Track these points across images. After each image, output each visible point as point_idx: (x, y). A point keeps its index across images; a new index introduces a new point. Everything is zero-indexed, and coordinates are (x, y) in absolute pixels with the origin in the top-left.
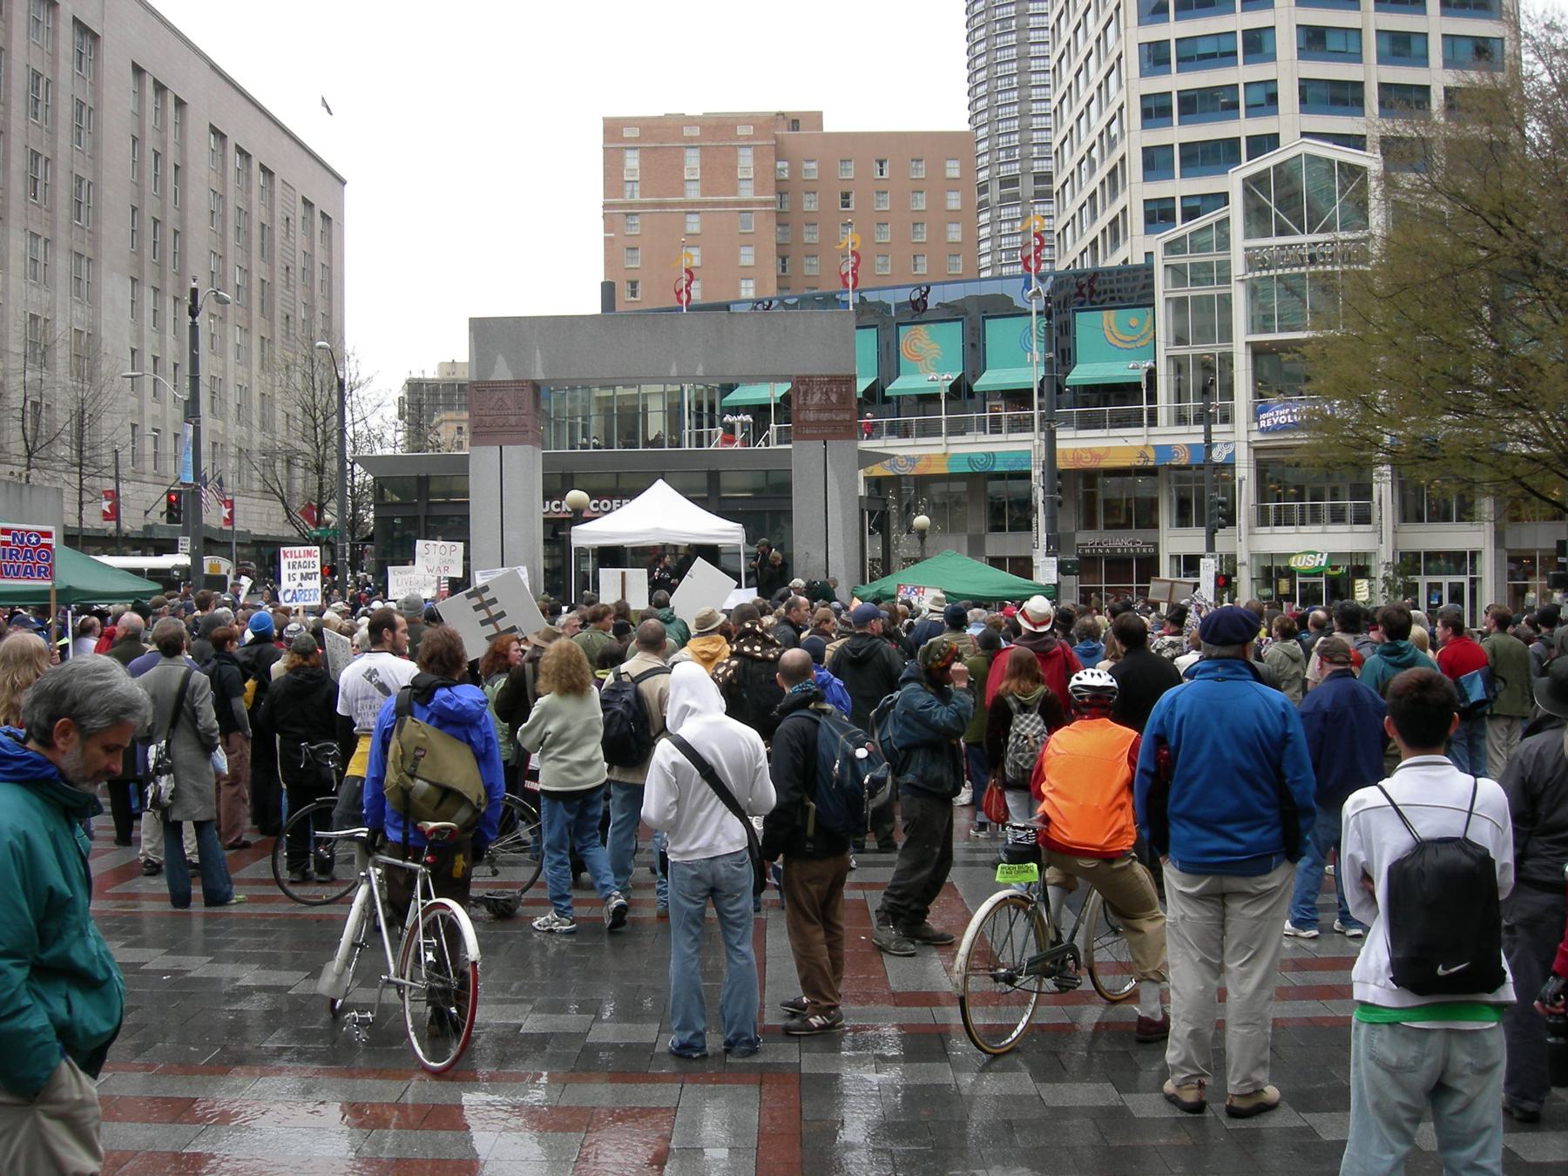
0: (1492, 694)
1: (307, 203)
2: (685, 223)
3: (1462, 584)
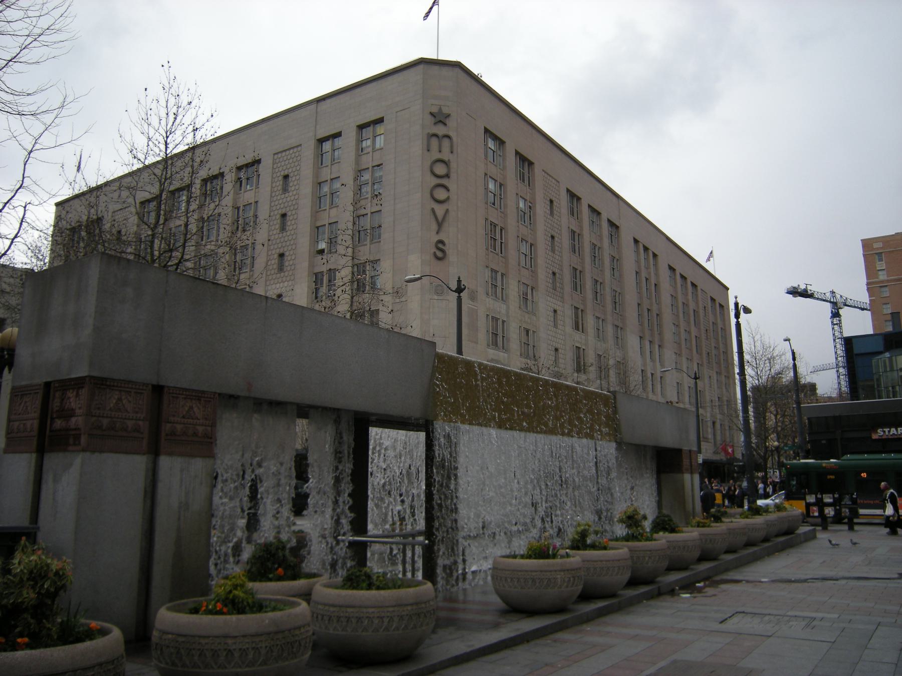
1: (713, 300)
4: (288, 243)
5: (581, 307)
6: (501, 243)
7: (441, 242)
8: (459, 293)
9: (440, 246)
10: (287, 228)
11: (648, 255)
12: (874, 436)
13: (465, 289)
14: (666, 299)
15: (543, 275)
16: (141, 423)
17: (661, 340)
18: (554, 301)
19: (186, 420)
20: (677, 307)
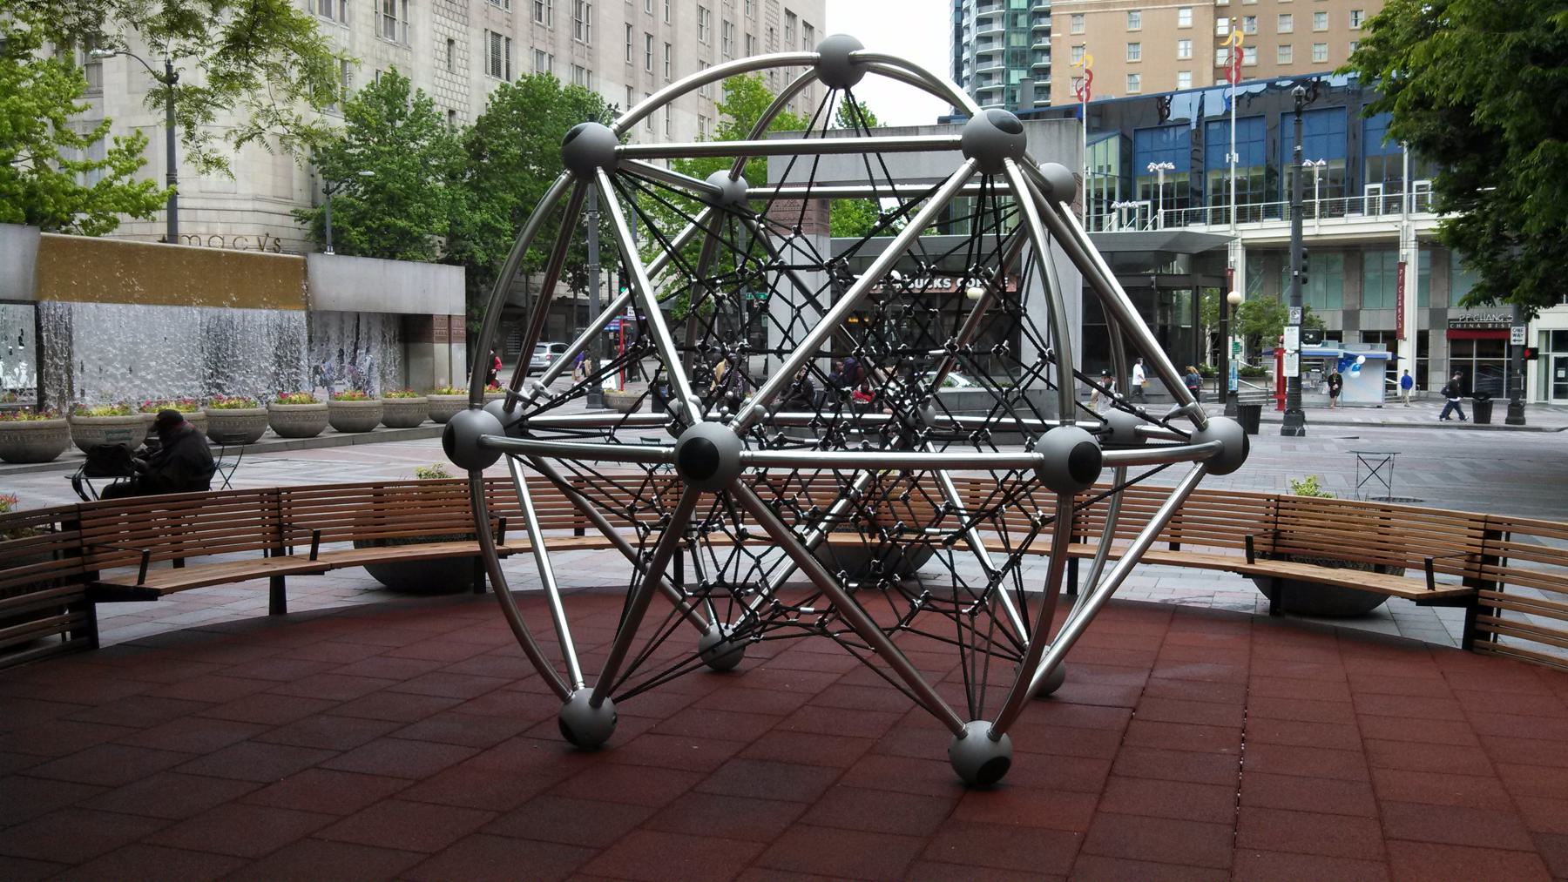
0: (428, 424)
1: (790, 14)
2: (1177, 18)
3: (1556, 358)
5: (506, 32)
18: (449, 22)
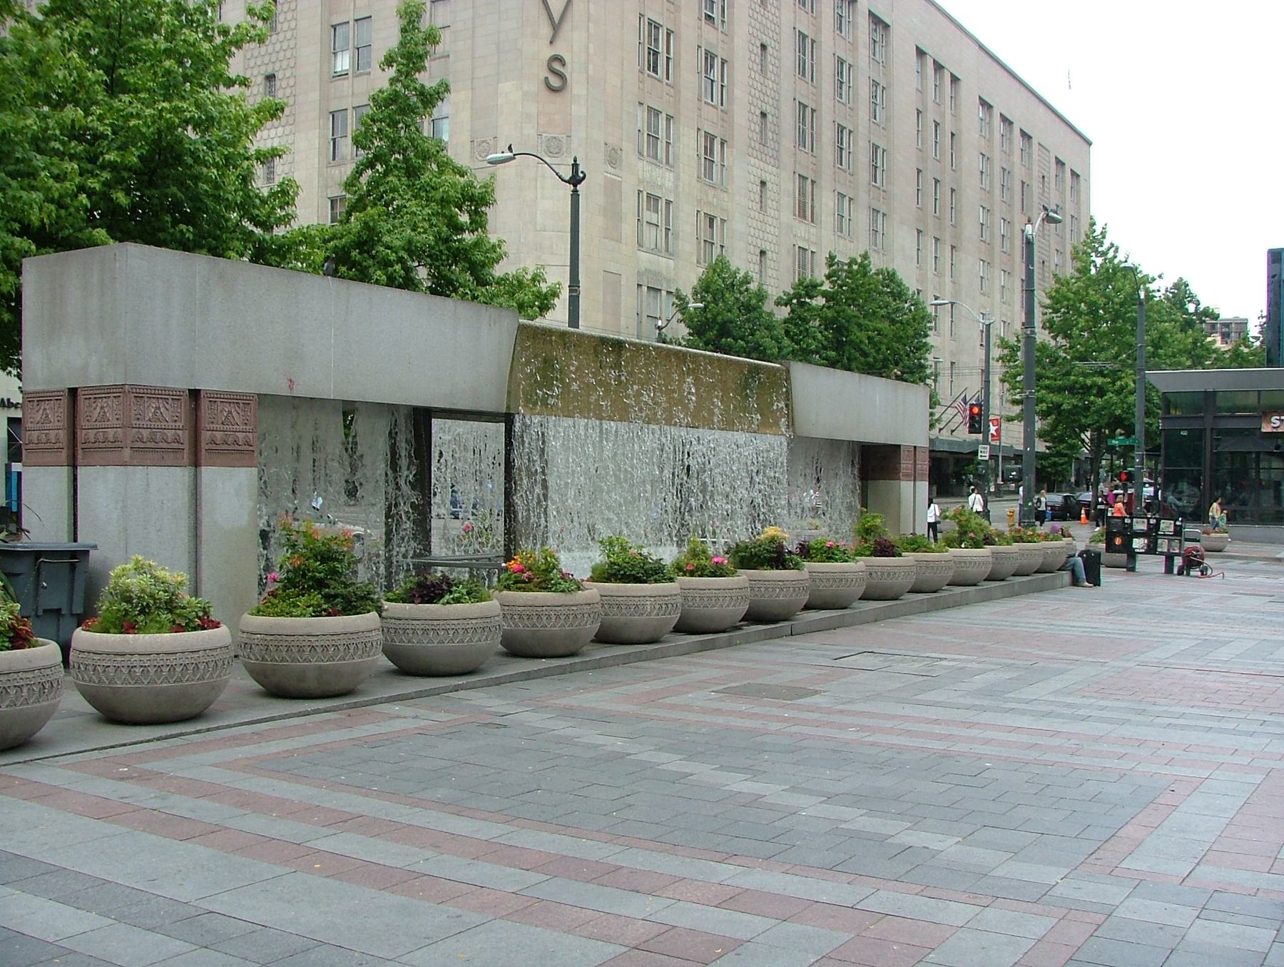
1: (1060, 163)
4: (281, 55)
6: (668, 58)
7: (558, 59)
8: (575, 186)
9: (557, 66)
10: (279, 26)
11: (942, 78)
12: (1266, 428)
13: (584, 178)
14: (971, 161)
15: (743, 118)
16: (180, 432)
17: (957, 236)
19: (215, 426)
20: (991, 176)
